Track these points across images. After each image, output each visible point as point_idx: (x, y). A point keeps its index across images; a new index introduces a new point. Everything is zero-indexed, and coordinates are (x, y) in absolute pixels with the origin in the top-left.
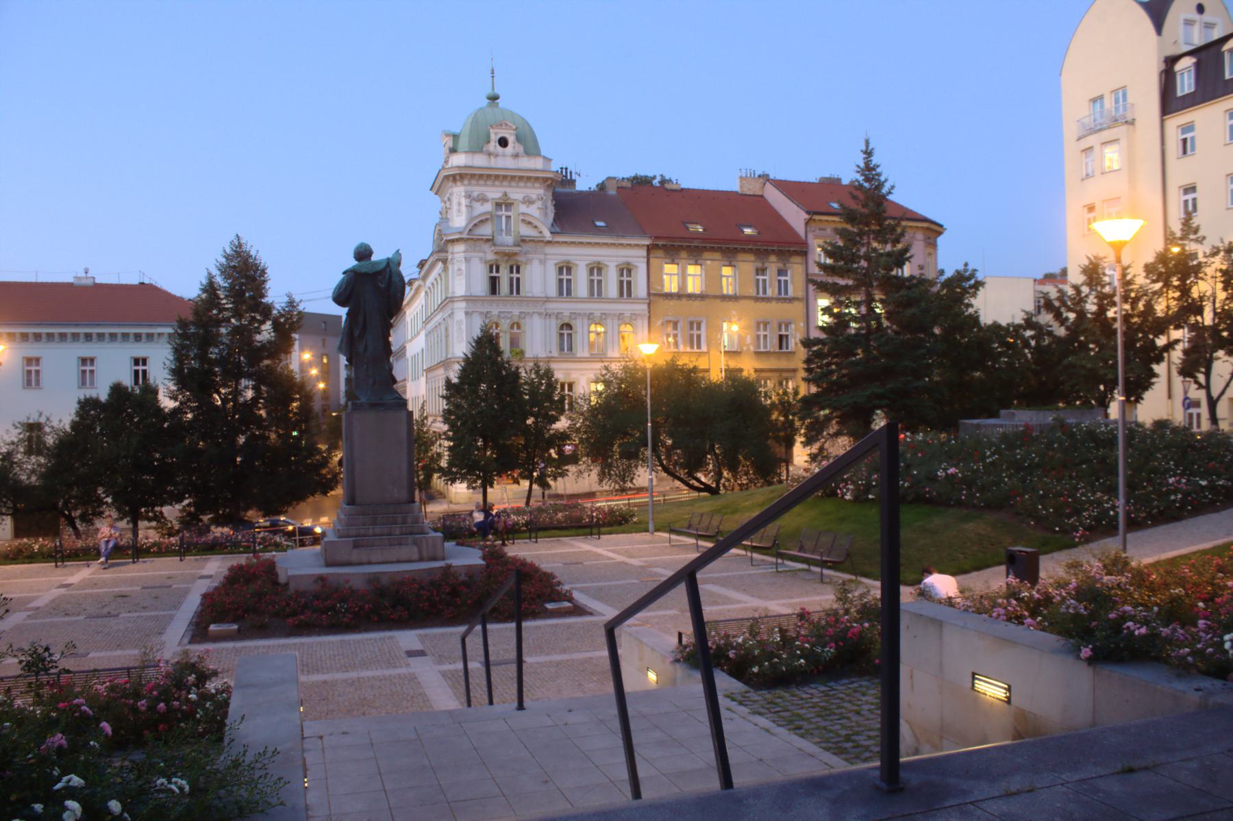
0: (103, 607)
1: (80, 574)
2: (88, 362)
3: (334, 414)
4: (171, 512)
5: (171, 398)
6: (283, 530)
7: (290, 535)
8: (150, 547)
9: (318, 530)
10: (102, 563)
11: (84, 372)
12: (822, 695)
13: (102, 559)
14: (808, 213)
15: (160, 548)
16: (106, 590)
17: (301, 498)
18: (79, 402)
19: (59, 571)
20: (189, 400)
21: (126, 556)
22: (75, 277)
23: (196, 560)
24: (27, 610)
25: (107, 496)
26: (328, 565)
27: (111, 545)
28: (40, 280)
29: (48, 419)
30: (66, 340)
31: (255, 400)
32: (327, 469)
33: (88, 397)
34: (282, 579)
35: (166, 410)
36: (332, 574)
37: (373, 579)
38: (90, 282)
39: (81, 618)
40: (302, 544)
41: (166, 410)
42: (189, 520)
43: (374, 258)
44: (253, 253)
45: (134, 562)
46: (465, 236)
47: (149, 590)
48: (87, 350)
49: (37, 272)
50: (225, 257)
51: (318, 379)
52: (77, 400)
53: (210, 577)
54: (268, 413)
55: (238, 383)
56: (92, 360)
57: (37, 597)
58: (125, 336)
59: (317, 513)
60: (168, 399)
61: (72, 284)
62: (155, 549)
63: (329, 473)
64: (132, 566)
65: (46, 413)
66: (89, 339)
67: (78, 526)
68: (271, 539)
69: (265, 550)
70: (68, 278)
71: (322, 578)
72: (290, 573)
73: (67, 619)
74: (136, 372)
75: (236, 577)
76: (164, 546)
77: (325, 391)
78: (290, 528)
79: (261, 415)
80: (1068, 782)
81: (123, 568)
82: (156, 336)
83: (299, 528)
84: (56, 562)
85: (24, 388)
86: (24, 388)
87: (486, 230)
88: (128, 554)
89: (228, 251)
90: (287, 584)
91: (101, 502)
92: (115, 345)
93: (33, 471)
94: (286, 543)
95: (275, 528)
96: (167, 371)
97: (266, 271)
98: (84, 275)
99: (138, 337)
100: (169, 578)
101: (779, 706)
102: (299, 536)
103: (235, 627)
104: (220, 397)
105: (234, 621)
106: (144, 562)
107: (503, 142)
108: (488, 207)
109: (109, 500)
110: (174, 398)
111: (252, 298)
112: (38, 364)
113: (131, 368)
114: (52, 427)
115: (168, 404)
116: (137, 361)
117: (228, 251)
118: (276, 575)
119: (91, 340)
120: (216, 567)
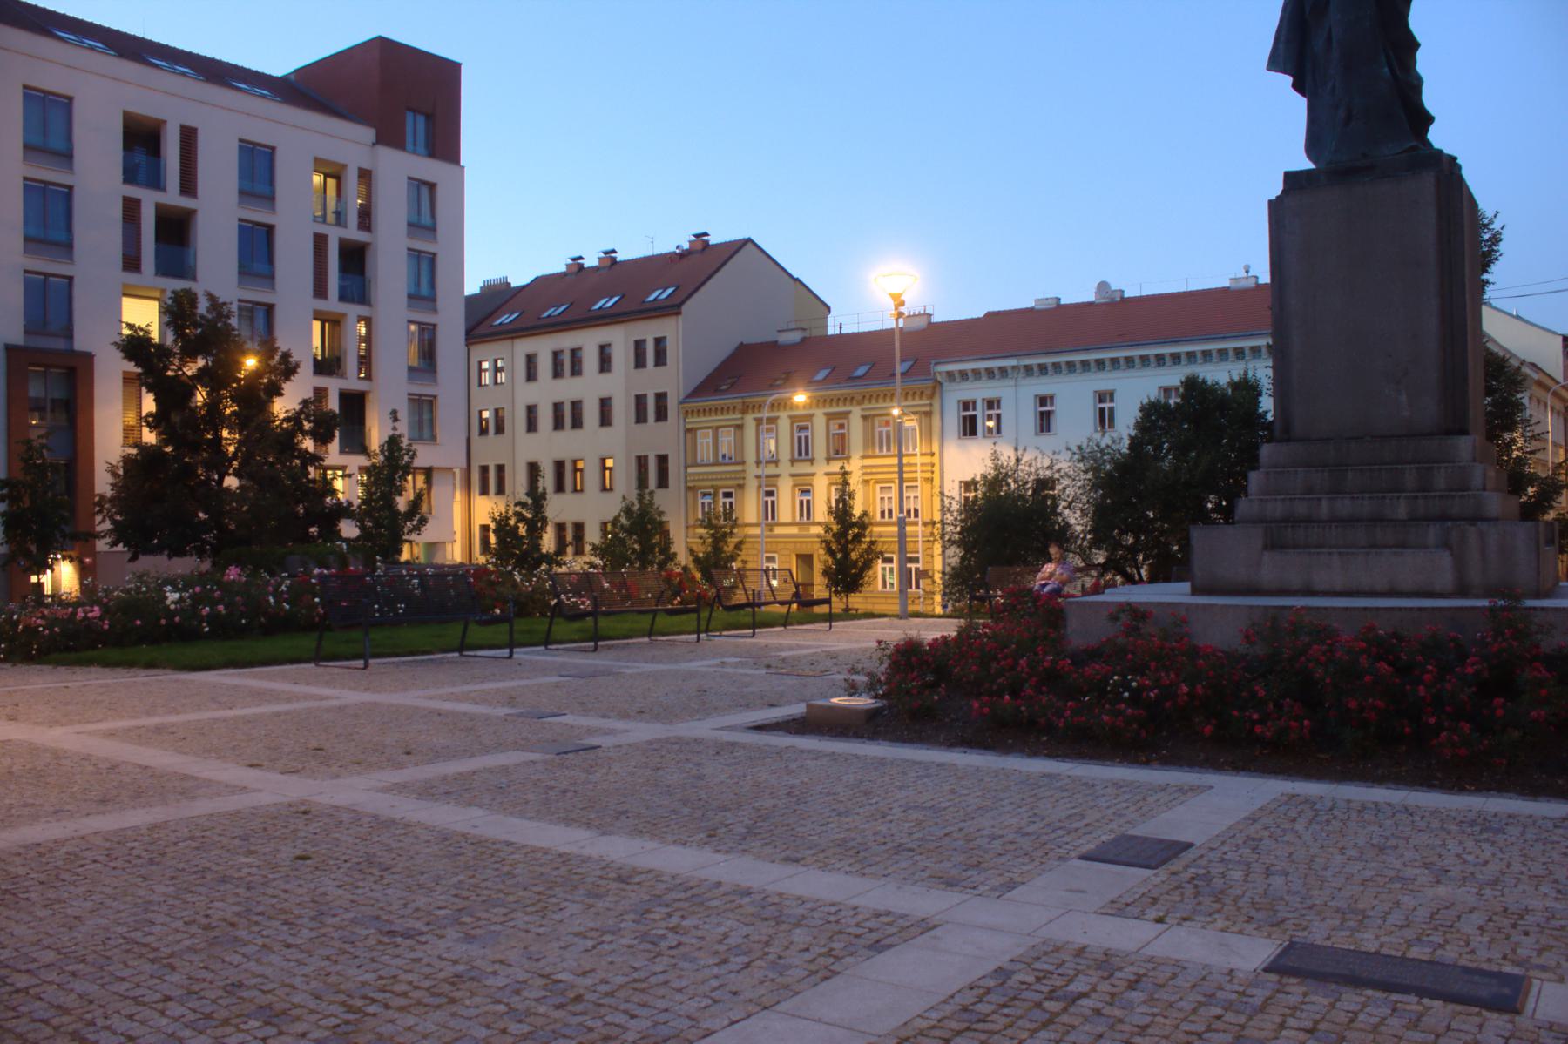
12: (202, 993)
28: (1191, 288)
30: (1211, 360)
38: (1251, 284)
48: (1043, 386)
58: (1145, 360)
61: (1228, 288)
66: (1192, 359)
70: (1224, 283)
80: (1046, 953)
85: (1036, 434)
86: (1036, 434)
92: (1073, 377)
101: (272, 982)
112: (1112, 400)
113: (1095, 406)
119: (1061, 372)
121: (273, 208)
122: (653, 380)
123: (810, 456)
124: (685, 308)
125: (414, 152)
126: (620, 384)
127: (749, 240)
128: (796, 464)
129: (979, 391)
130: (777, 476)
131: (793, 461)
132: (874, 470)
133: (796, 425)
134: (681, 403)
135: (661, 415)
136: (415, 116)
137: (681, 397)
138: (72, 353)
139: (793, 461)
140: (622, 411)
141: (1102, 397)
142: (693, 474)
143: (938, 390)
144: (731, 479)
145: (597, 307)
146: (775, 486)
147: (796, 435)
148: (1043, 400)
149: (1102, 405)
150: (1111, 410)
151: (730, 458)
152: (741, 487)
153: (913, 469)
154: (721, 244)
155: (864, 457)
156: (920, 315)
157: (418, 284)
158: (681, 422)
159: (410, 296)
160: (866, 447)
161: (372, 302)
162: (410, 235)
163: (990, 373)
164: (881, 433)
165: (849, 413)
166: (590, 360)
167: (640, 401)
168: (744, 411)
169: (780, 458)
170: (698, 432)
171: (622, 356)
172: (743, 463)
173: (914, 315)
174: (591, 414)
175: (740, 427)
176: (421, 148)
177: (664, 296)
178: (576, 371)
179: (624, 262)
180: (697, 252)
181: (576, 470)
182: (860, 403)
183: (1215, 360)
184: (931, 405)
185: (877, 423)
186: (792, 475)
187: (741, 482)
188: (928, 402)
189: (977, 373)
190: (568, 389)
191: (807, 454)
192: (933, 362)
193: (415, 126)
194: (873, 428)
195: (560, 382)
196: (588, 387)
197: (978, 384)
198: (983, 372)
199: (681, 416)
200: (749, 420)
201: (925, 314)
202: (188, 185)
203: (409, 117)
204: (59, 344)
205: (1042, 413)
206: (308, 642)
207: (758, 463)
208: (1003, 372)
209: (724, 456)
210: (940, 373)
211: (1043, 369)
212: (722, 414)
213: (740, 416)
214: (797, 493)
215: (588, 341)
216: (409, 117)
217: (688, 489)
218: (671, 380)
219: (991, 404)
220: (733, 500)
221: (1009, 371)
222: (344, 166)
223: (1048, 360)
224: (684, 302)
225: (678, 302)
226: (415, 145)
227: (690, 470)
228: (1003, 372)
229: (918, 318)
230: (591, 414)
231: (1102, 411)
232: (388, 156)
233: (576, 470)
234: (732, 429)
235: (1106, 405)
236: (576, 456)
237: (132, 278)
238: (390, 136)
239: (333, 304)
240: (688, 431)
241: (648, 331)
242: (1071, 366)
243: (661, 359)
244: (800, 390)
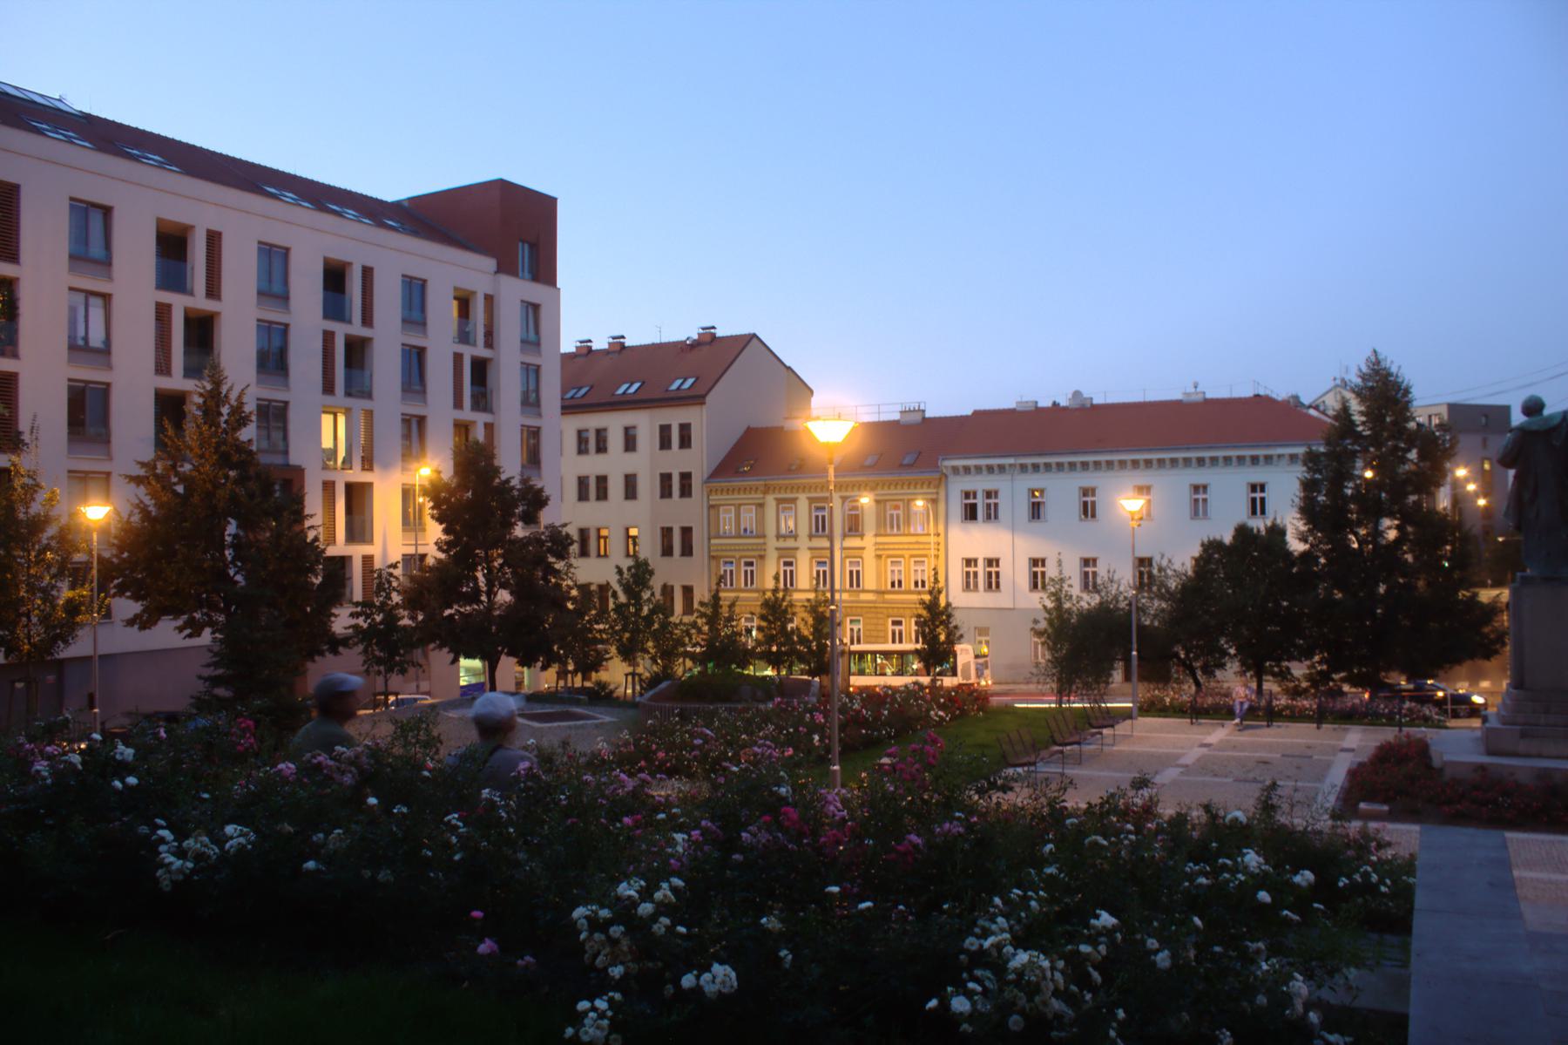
0: (1249, 771)
1: (1219, 734)
2: (1201, 490)
3: (1500, 539)
4: (1299, 670)
5: (1300, 540)
6: (1433, 696)
7: (1440, 703)
8: (1283, 710)
9: (1478, 699)
10: (1237, 725)
11: (1196, 501)
13: (1237, 721)
15: (1292, 712)
16: (1247, 754)
17: (1458, 661)
18: (1203, 545)
19: (1195, 728)
20: (1320, 542)
21: (1257, 718)
22: (1185, 394)
23: (1334, 729)
24: (1178, 766)
25: (1231, 647)
26: (1490, 753)
27: (1246, 706)
29: (1170, 561)
31: (1398, 541)
32: (1490, 628)
33: (1211, 539)
34: (1436, 763)
35: (1296, 554)
36: (1491, 764)
37: (1544, 774)
38: (1199, 398)
39: (1230, 780)
40: (1456, 715)
41: (1296, 554)
42: (1318, 680)
43: (1546, 412)
44: (1394, 370)
45: (1268, 726)
47: (1290, 759)
48: (1035, 480)
49: (1144, 390)
50: (1360, 377)
51: (1476, 495)
52: (1200, 542)
53: (1352, 750)
54: (1415, 558)
55: (1377, 524)
56: (1205, 488)
57: (1183, 754)
59: (1475, 678)
60: (1297, 541)
62: (1288, 712)
63: (1492, 631)
64: (1267, 731)
65: (1168, 555)
67: (1199, 677)
68: (1419, 711)
69: (1411, 724)
70: (1175, 395)
71: (1482, 768)
72: (1447, 758)
73: (1216, 780)
74: (1254, 500)
75: (1385, 755)
76: (1297, 710)
77: (1486, 508)
78: (1440, 694)
79: (1406, 560)
81: (1258, 731)
82: (1275, 458)
83: (1452, 695)
84: (1191, 718)
86: (1029, 521)
88: (1258, 716)
89: (1365, 369)
90: (1441, 770)
91: (1224, 653)
93: (1155, 616)
94: (1437, 717)
95: (1425, 698)
96: (1296, 509)
97: (1412, 390)
98: (1193, 390)
99: (1255, 460)
100: (1309, 747)
102: (1452, 704)
103: (1386, 808)
104: (1357, 539)
105: (1384, 802)
106: (1279, 727)
109: (1232, 651)
110: (1303, 539)
111: (1394, 423)
114: (1175, 571)
115: (1296, 546)
116: (1253, 488)
117: (1365, 369)
118: (1430, 758)
120: (1359, 741)
121: (424, 332)
122: (677, 461)
124: (709, 399)
125: (523, 278)
126: (646, 463)
127: (754, 336)
128: (813, 539)
129: (980, 484)
130: (797, 549)
131: (811, 537)
132: (886, 547)
134: (706, 482)
135: (686, 491)
137: (706, 476)
138: (288, 467)
139: (811, 537)
140: (648, 486)
141: (1086, 492)
142: (715, 545)
143: (943, 479)
144: (753, 550)
145: (620, 391)
146: (794, 557)
147: (814, 514)
148: (1086, 492)
149: (1085, 499)
150: (1093, 503)
151: (752, 532)
152: (762, 557)
153: (927, 546)
154: (727, 337)
155: (876, 535)
156: (914, 411)
158: (705, 499)
160: (878, 525)
161: (494, 406)
162: (523, 351)
163: (990, 469)
164: (892, 516)
166: (615, 440)
167: (666, 479)
168: (767, 490)
169: (799, 532)
170: (721, 509)
172: (764, 536)
173: (910, 411)
174: (616, 487)
175: (761, 506)
176: (527, 274)
178: (602, 448)
179: (633, 347)
181: (599, 537)
182: (804, 491)
183: (1180, 466)
184: (937, 493)
185: (888, 507)
186: (810, 549)
187: (762, 553)
188: (934, 491)
189: (978, 469)
192: (941, 458)
194: (885, 511)
195: (584, 458)
196: (614, 464)
197: (979, 478)
198: (984, 468)
200: (770, 500)
201: (919, 410)
202: (367, 320)
204: (277, 460)
205: (1033, 504)
207: (779, 536)
208: (1002, 468)
209: (745, 530)
210: (946, 467)
211: (1036, 467)
212: (745, 493)
213: (761, 496)
214: (814, 564)
215: (614, 423)
217: (712, 558)
218: (697, 461)
219: (989, 494)
220: (754, 568)
221: (1007, 468)
222: (474, 293)
223: (1041, 460)
224: (706, 394)
225: (704, 393)
227: (713, 541)
228: (1002, 468)
229: (912, 414)
230: (616, 487)
231: (1085, 504)
232: (506, 281)
233: (599, 537)
234: (754, 507)
235: (1089, 499)
236: (598, 525)
237: (329, 399)
238: (506, 267)
239: (467, 414)
240: (711, 507)
241: (674, 417)
242: (1060, 466)
243: (685, 442)
244: (865, 493)
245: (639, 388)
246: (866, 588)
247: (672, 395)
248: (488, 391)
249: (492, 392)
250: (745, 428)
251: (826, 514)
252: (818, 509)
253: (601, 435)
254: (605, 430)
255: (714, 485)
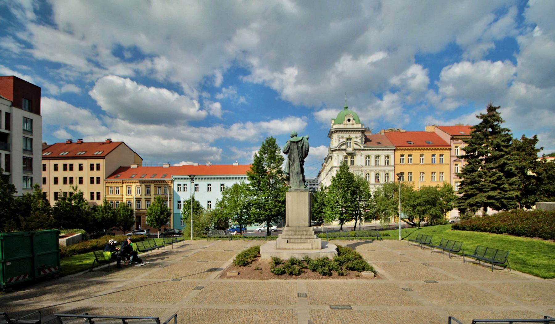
14: (452, 136)
46: (337, 148)
87: (344, 147)
107: (349, 120)
108: (345, 140)
123: (131, 194)
125: (25, 110)
126: (86, 174)
127: (123, 142)
131: (145, 195)
133: (127, 187)
136: (25, 100)
139: (145, 195)
145: (78, 154)
148: (209, 185)
157: (26, 146)
159: (24, 150)
165: (151, 185)
166: (76, 167)
171: (61, 167)
176: (28, 110)
177: (48, 154)
180: (108, 143)
182: (153, 183)
190: (68, 174)
191: (149, 193)
193: (26, 103)
195: (65, 172)
197: (182, 181)
199: (105, 183)
203: (23, 100)
206: (334, 229)
215: (76, 163)
216: (23, 100)
219: (184, 185)
225: (104, 155)
226: (25, 108)
227: (107, 196)
241: (95, 162)
245: (84, 154)
246: (142, 208)
247: (95, 156)
248: (8, 144)
249: (9, 144)
250: (119, 166)
251: (113, 189)
252: (128, 188)
253: (71, 166)
254: (57, 165)
255: (109, 180)
